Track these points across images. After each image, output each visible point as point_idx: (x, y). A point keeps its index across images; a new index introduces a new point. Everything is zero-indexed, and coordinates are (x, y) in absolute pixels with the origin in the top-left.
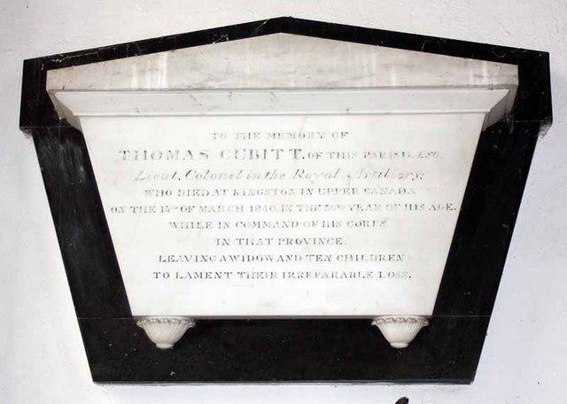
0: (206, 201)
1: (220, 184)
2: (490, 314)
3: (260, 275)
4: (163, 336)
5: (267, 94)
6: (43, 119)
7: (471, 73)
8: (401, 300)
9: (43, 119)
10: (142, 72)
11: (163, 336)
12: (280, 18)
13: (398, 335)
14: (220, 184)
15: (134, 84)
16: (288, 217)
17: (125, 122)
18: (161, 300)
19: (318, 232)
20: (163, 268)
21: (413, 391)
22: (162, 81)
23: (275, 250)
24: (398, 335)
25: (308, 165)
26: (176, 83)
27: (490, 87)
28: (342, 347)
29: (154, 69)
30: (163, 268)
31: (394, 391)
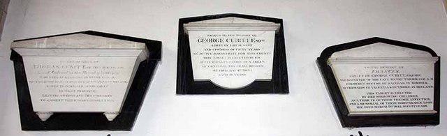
0: (58, 80)
1: (62, 75)
2: (188, 94)
3: (72, 100)
4: (43, 117)
5: (74, 51)
6: (16, 58)
7: (132, 45)
8: (112, 108)
9: (16, 58)
10: (40, 43)
11: (43, 117)
12: (116, 130)
13: (110, 117)
14: (62, 75)
15: (36, 47)
16: (80, 84)
17: (35, 58)
18: (43, 106)
19: (87, 89)
20: (44, 98)
21: (112, 133)
22: (44, 46)
23: (76, 94)
24: (110, 117)
25: (87, 70)
26: (48, 46)
27: (136, 52)
28: (96, 120)
29: (42, 43)
30: (44, 98)
31: (107, 133)
